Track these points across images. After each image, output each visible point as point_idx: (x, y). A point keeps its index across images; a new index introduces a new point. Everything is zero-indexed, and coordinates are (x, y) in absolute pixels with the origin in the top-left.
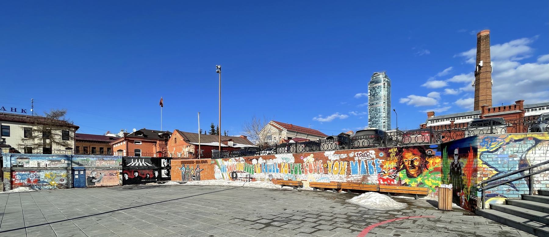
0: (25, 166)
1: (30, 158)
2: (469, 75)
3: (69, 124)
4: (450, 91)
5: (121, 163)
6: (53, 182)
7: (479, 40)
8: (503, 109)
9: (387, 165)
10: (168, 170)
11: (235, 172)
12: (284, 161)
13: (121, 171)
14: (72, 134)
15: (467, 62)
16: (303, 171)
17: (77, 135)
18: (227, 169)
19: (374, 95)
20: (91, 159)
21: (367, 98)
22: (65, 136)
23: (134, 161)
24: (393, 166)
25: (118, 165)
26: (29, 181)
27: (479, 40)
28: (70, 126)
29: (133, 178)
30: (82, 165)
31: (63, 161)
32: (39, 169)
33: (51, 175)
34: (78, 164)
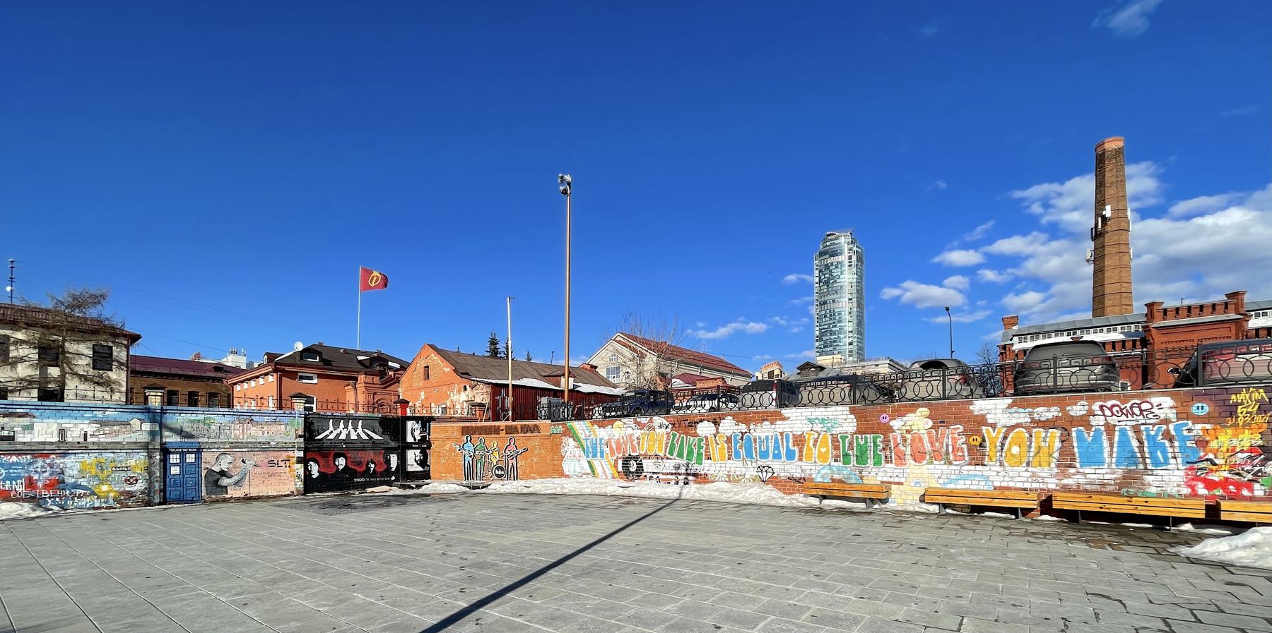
0: (20, 438)
1: (36, 413)
2: (1029, 238)
3: (113, 328)
4: (990, 275)
5: (301, 432)
6: (105, 488)
7: (1101, 160)
8: (1198, 311)
9: (1224, 439)
10: (424, 452)
11: (636, 458)
12: (818, 428)
13: (301, 454)
14: (120, 353)
15: (1027, 211)
16: (889, 454)
17: (133, 359)
18: (607, 450)
19: (827, 283)
20: (218, 419)
21: (811, 286)
22: (102, 360)
23: (336, 426)
24: (1246, 444)
25: (291, 438)
26: (31, 484)
27: (1101, 160)
28: (116, 333)
29: (336, 475)
30: (192, 436)
31: (135, 423)
32: (63, 448)
33: (100, 466)
34: (180, 432)
